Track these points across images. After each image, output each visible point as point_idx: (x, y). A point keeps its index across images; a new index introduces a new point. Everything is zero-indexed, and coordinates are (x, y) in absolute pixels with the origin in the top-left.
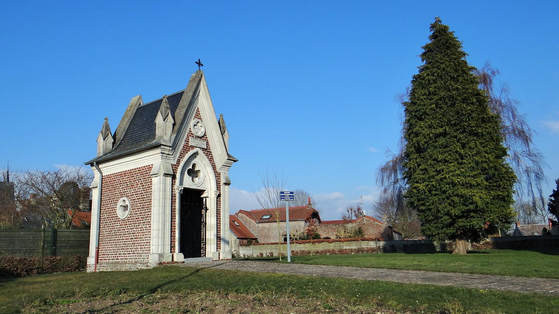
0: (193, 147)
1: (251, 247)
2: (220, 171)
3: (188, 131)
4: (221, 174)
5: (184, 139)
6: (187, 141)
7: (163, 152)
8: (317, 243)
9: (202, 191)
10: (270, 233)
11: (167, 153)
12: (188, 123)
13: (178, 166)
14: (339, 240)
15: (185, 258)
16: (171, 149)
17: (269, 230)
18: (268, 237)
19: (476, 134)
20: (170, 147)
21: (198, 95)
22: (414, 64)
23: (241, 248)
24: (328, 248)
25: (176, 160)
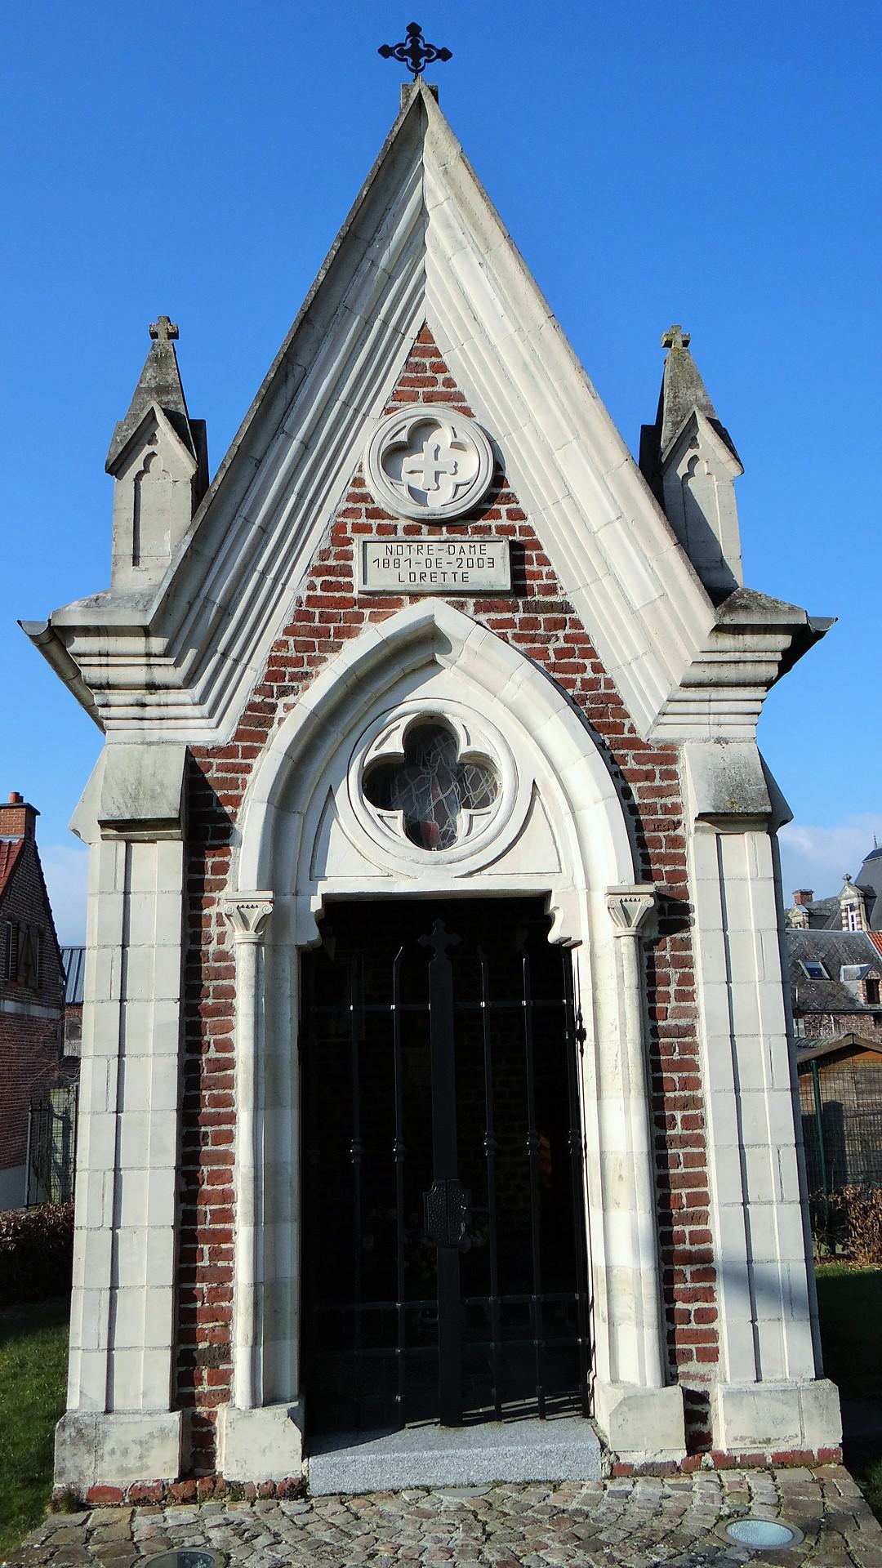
0: (383, 602)
2: (665, 733)
3: (335, 499)
5: (308, 555)
9: (533, 909)
11: (140, 675)
12: (324, 452)
13: (251, 753)
15: (308, 1451)
16: (158, 644)
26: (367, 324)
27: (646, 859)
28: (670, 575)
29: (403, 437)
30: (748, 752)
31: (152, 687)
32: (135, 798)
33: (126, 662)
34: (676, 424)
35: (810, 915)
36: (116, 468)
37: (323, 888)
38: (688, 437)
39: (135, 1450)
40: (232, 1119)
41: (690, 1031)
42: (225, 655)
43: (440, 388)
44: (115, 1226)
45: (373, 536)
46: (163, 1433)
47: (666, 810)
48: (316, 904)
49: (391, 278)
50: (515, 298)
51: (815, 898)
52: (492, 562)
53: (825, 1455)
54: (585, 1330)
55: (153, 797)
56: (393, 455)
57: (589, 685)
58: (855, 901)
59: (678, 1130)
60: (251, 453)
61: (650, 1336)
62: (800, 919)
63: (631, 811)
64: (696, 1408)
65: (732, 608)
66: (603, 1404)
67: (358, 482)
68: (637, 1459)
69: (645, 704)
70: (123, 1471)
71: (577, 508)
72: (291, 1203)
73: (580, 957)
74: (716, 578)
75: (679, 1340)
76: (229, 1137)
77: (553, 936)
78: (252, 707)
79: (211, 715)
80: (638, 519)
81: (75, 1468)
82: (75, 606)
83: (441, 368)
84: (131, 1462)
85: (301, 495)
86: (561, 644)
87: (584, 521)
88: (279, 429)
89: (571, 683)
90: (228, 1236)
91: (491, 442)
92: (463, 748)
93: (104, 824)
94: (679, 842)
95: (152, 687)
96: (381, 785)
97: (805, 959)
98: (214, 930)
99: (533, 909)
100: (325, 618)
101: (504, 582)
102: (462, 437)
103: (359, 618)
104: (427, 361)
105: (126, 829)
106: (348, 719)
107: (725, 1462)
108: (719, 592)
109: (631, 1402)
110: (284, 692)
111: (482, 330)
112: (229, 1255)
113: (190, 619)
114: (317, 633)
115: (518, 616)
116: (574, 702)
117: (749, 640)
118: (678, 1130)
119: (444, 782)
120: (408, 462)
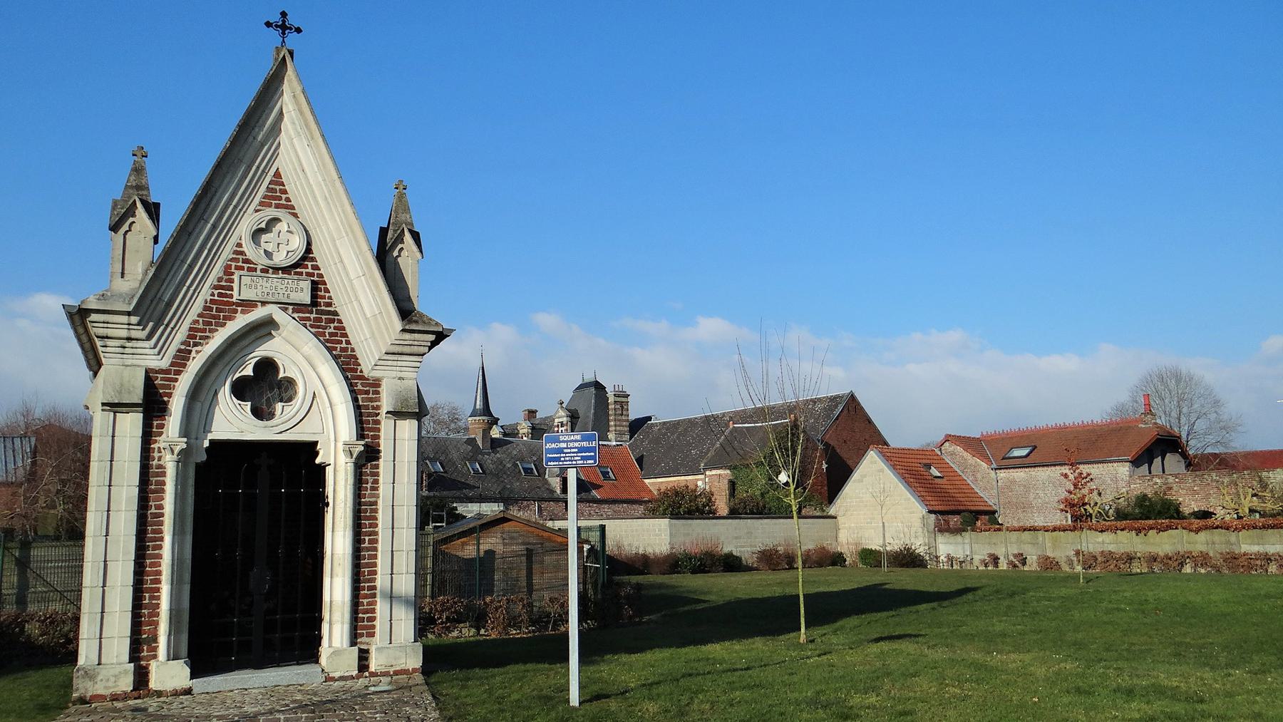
0: (248, 305)
1: (967, 535)
3: (227, 253)
5: (212, 279)
6: (224, 287)
9: (310, 448)
10: (1032, 496)
11: (124, 333)
12: (222, 229)
13: (178, 373)
14: (1241, 524)
15: (192, 678)
16: (134, 319)
17: (1027, 488)
18: (1026, 507)
20: (129, 314)
21: (276, 129)
24: (1188, 547)
25: (172, 351)
26: (249, 168)
27: (363, 429)
28: (384, 305)
29: (263, 225)
30: (412, 384)
31: (129, 339)
32: (120, 393)
33: (119, 327)
34: (395, 231)
35: (533, 428)
36: (114, 228)
37: (210, 436)
38: (400, 239)
39: (113, 679)
40: (162, 539)
41: (375, 503)
42: (167, 325)
43: (283, 202)
44: (104, 586)
45: (244, 272)
46: (126, 672)
47: (373, 408)
48: (206, 444)
49: (263, 146)
50: (324, 165)
51: (538, 415)
52: (302, 290)
53: (415, 670)
54: (320, 630)
55: (129, 393)
56: (257, 234)
57: (343, 350)
58: (565, 420)
59: (366, 545)
60: (186, 231)
61: (347, 627)
62: (525, 431)
63: (357, 408)
64: (364, 656)
65: (410, 322)
66: (325, 651)
67: (239, 245)
68: (337, 675)
69: (368, 364)
70: (106, 688)
71: (345, 268)
72: (187, 576)
73: (329, 471)
74: (405, 305)
75: (360, 625)
76: (160, 547)
77: (318, 461)
78: (179, 351)
79: (156, 350)
80: (374, 281)
81: (83, 687)
82: (92, 298)
83: (285, 192)
84: (110, 684)
85: (210, 251)
86: (332, 330)
87: (347, 275)
88: (201, 218)
89: (335, 349)
90: (158, 590)
91: (306, 231)
92: (281, 375)
93: (103, 404)
94: (378, 422)
95: (129, 339)
96: (241, 389)
97: (522, 461)
98: (156, 455)
99: (310, 448)
100: (218, 310)
101: (308, 300)
102: (292, 228)
103: (236, 312)
104: (278, 188)
105: (114, 407)
106: (227, 359)
107: (373, 674)
108: (406, 311)
109: (336, 653)
110: (196, 345)
111: (306, 177)
112: (158, 598)
113: (152, 307)
114: (214, 317)
115: (312, 316)
116: (335, 358)
117: (417, 336)
118: (366, 545)
119: (271, 389)
120: (264, 237)
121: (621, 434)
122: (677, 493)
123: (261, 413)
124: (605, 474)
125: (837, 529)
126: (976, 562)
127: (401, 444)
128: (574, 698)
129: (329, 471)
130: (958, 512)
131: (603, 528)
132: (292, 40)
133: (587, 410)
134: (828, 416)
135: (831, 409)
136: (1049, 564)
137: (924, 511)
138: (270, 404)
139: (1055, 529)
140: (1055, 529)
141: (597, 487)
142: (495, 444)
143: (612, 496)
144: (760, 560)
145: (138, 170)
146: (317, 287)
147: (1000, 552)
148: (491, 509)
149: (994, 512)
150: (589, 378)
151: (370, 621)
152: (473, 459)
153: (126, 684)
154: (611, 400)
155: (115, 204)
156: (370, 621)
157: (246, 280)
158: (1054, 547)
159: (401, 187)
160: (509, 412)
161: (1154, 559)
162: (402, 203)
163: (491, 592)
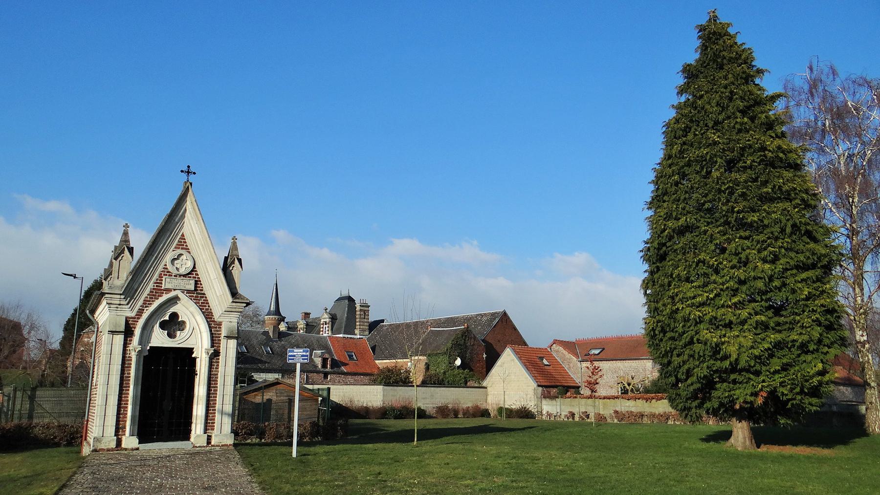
0: (168, 290)
2: (220, 320)
3: (160, 268)
4: (223, 324)
5: (154, 280)
6: (159, 283)
7: (109, 302)
8: (654, 401)
9: (191, 351)
12: (159, 259)
16: (123, 297)
19: (742, 225)
21: (183, 216)
22: (664, 101)
23: (544, 402)
25: (136, 310)
35: (307, 325)
38: (233, 262)
51: (311, 316)
58: (328, 320)
61: (203, 426)
63: (212, 334)
64: (209, 438)
74: (234, 291)
96: (163, 326)
99: (191, 351)
105: (113, 332)
108: (234, 293)
109: (198, 436)
116: (203, 313)
121: (362, 331)
122: (389, 370)
123: (171, 335)
124: (350, 357)
125: (487, 395)
126: (563, 417)
127: (229, 349)
128: (294, 455)
129: (198, 361)
130: (555, 385)
131: (329, 389)
132: (192, 178)
133: (342, 315)
134: (489, 325)
135: (491, 321)
136: (601, 418)
137: (535, 385)
138: (174, 332)
139: (604, 398)
140: (604, 398)
141: (345, 365)
142: (281, 335)
143: (354, 370)
144: (437, 412)
145: (126, 234)
146: (197, 283)
147: (575, 410)
148: (271, 377)
149: (579, 387)
150: (345, 294)
151: (212, 419)
152: (266, 345)
153: (113, 445)
154: (358, 308)
155: (116, 247)
156: (212, 419)
157: (168, 280)
158: (604, 409)
159: (234, 238)
160: (292, 313)
161: (653, 416)
162: (234, 247)
163: (269, 420)
